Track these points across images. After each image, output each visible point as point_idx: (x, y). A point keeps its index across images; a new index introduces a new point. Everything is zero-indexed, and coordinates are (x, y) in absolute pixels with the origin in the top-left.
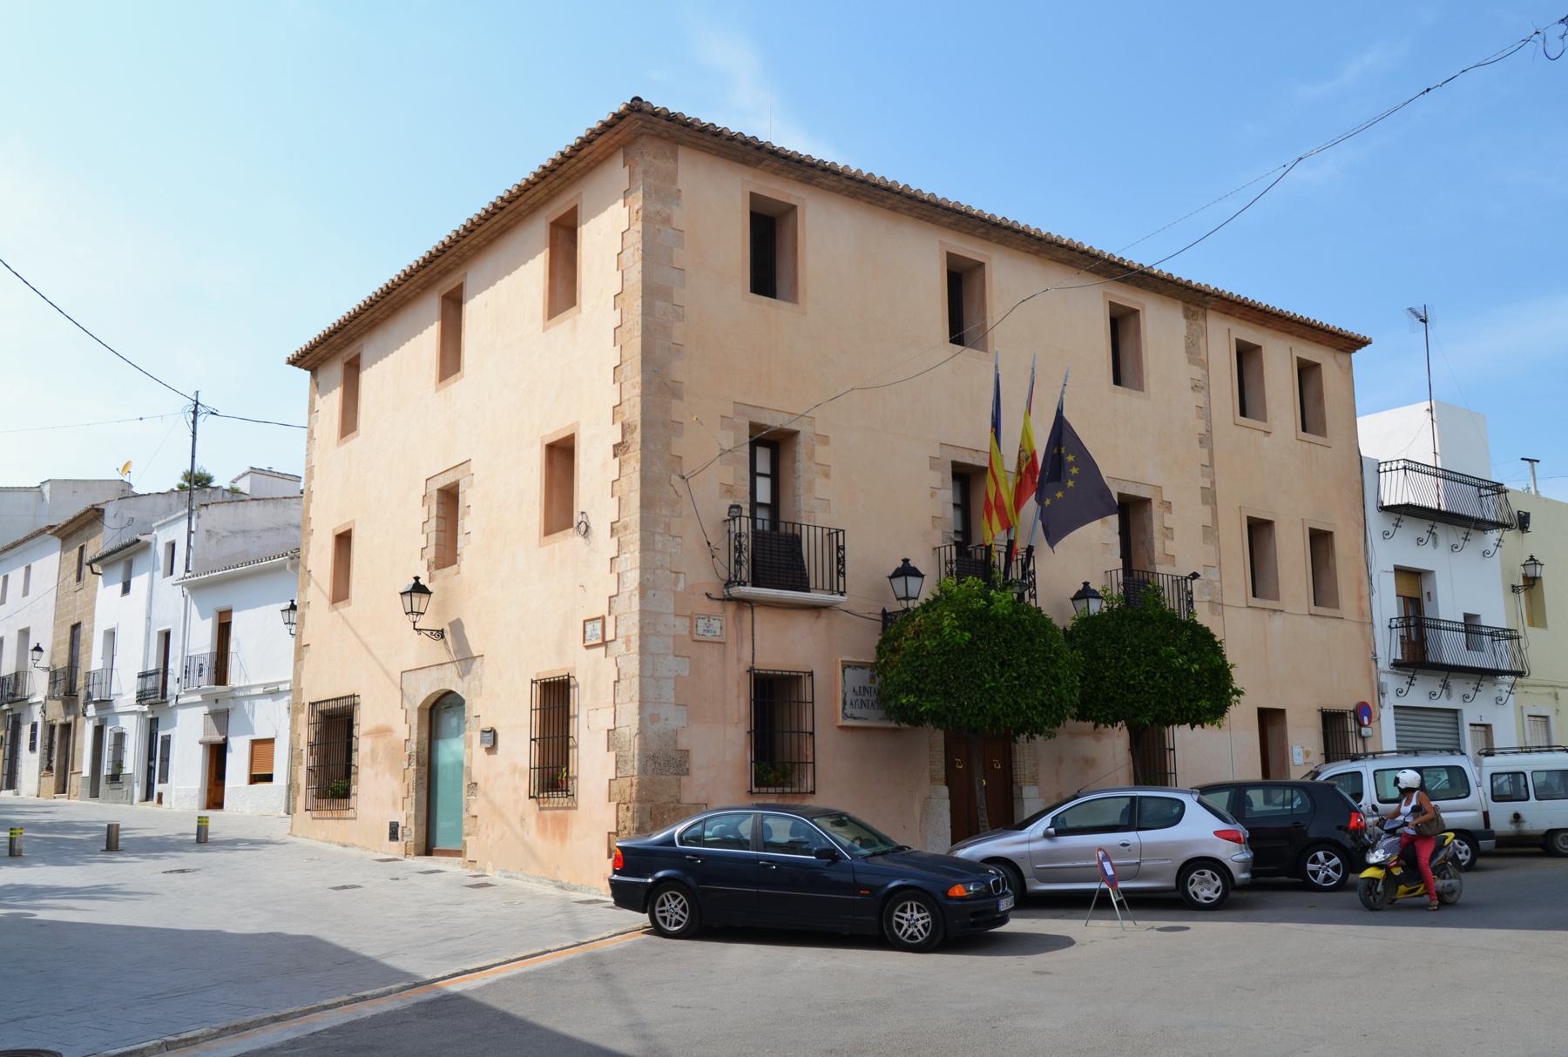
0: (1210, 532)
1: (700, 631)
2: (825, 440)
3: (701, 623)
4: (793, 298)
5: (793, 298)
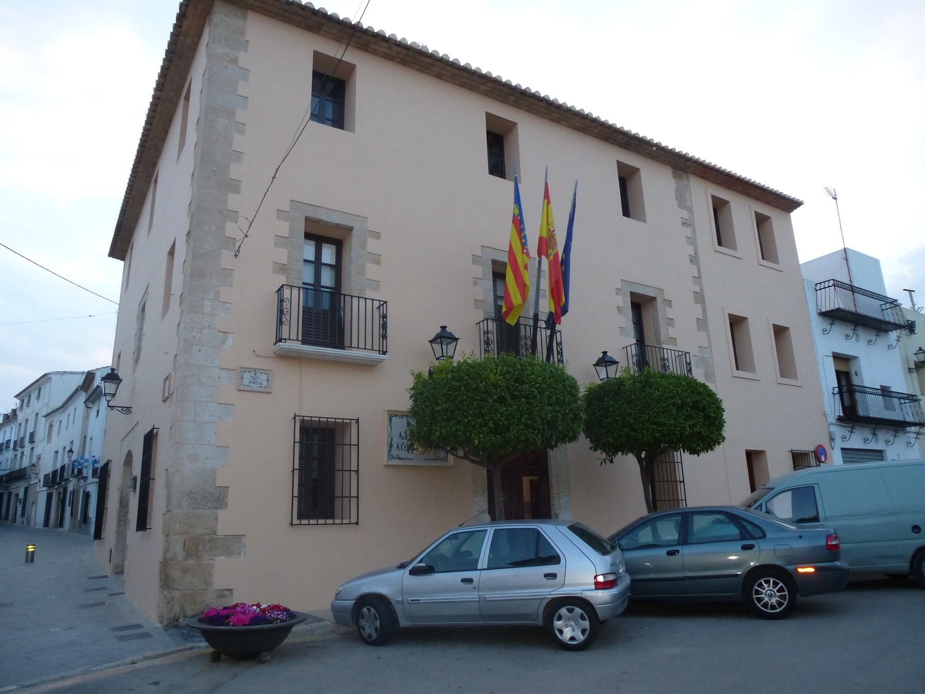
0: (702, 324)
1: (246, 382)
2: (377, 235)
3: (247, 376)
4: (352, 130)
5: (352, 130)
